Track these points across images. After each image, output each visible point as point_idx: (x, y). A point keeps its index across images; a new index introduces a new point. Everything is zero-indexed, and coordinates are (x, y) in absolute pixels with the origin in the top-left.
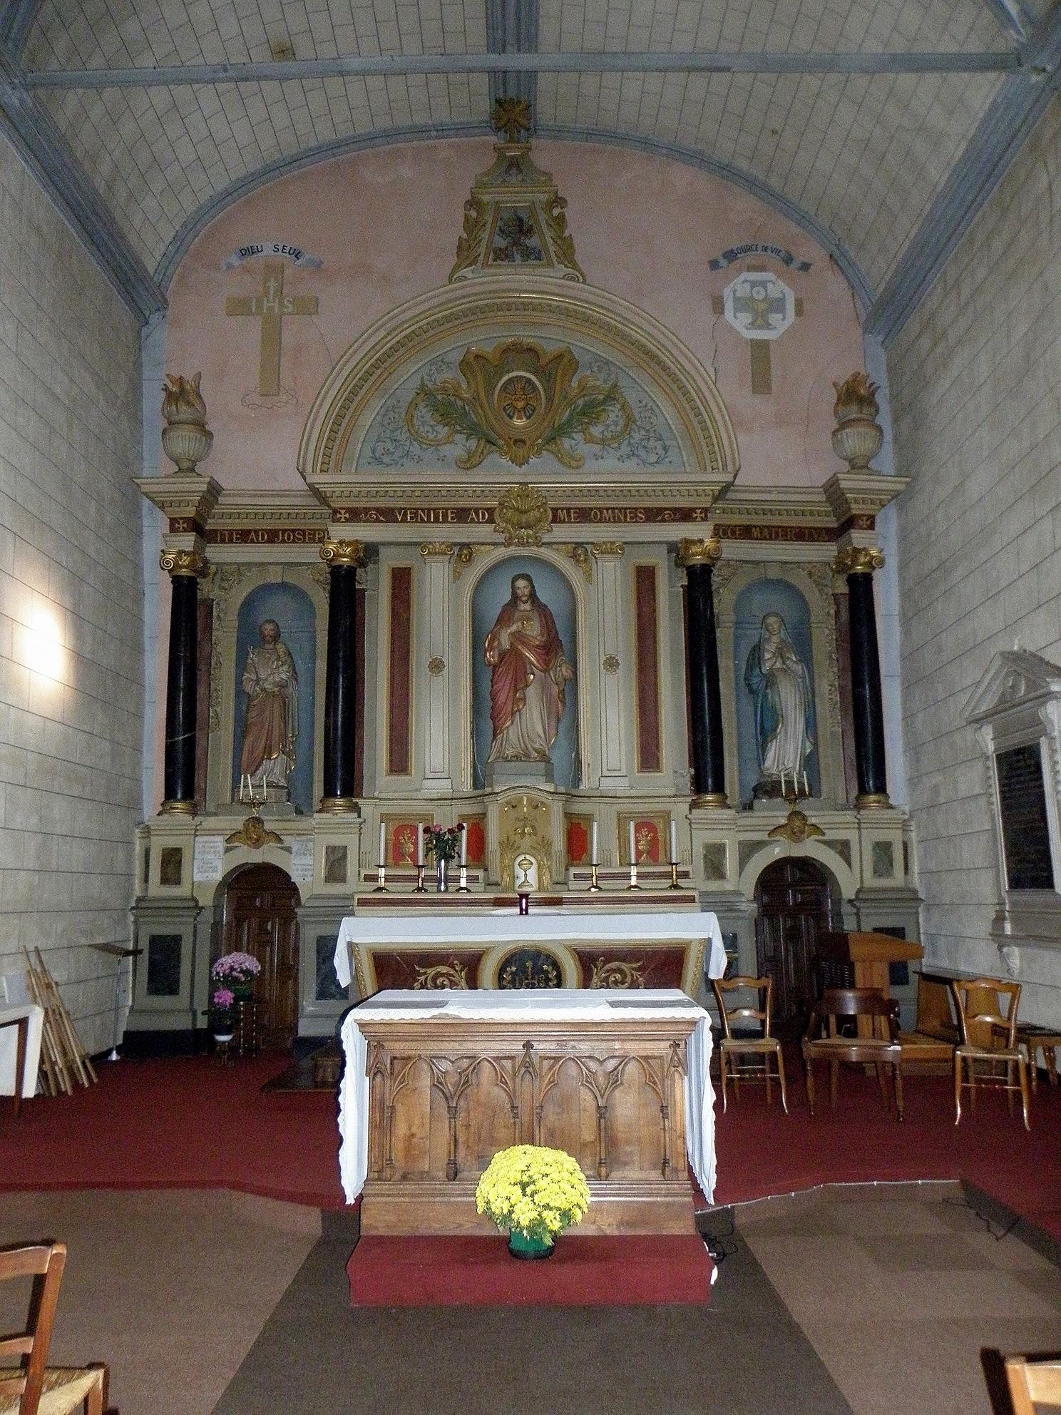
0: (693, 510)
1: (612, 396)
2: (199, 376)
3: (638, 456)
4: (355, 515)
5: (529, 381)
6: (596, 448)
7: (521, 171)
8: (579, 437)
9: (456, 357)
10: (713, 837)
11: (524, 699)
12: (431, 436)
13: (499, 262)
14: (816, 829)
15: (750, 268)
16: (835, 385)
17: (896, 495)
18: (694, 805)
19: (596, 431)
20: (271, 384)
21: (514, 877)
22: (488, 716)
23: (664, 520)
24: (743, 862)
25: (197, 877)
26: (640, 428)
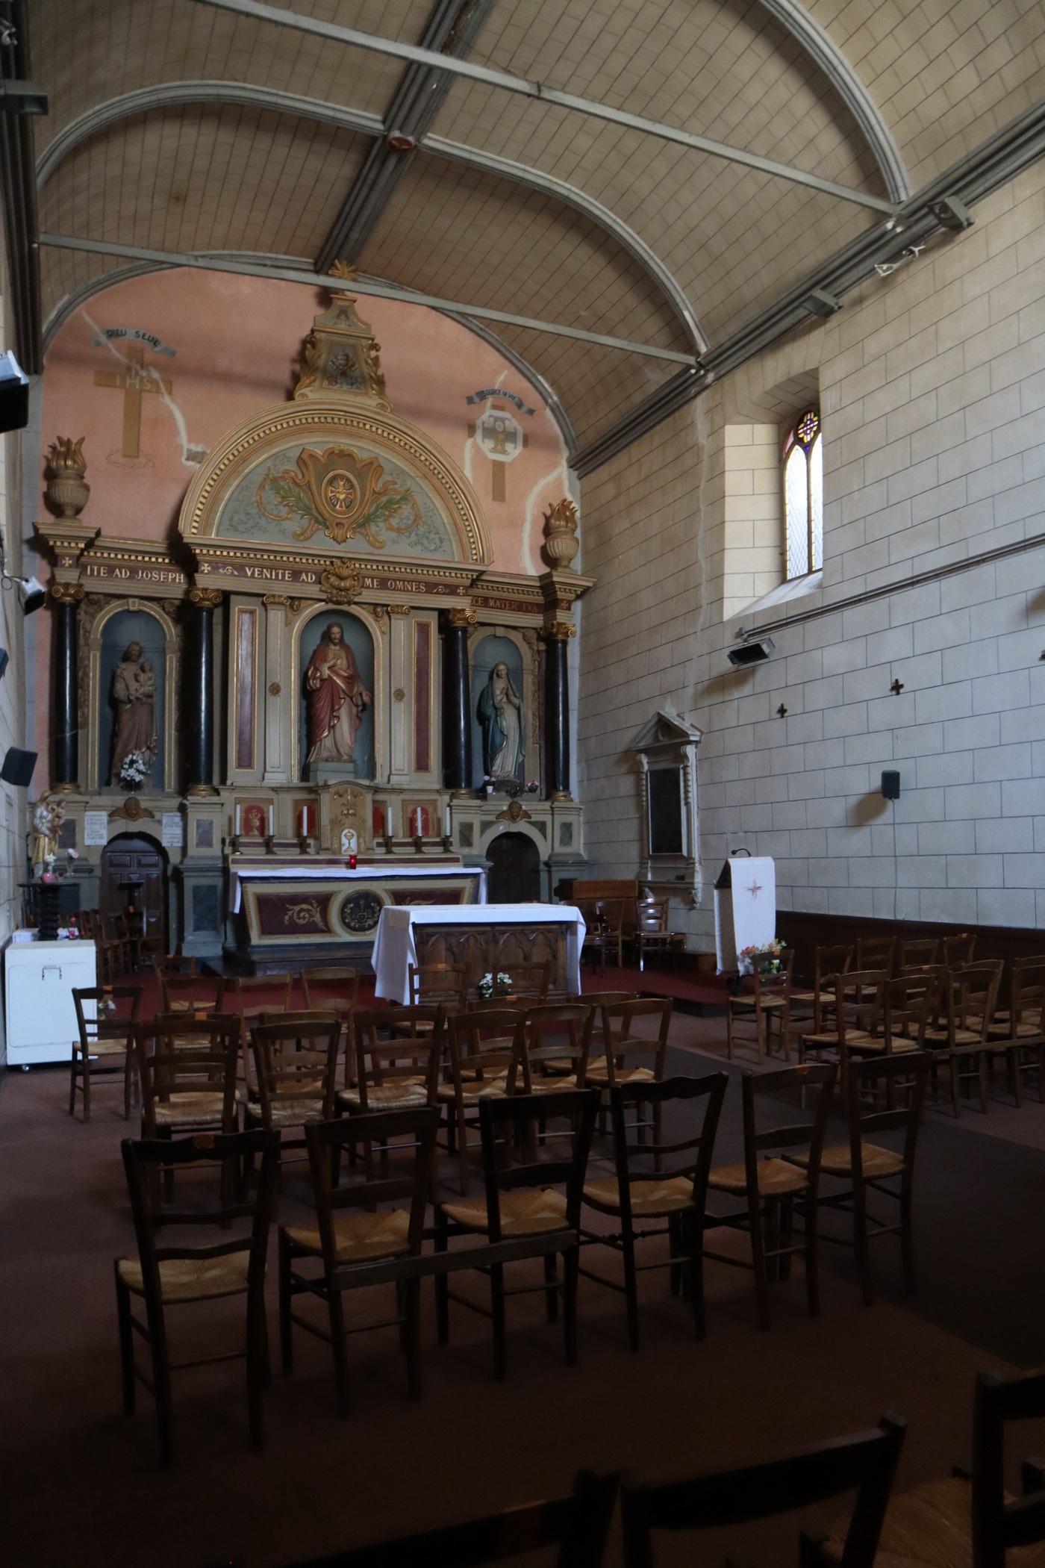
0: (458, 587)
1: (405, 497)
2: (82, 440)
4: (215, 567)
5: (348, 480)
6: (394, 535)
8: (381, 525)
9: (295, 454)
10: (466, 818)
11: (338, 718)
14: (527, 815)
15: (494, 407)
17: (586, 590)
18: (453, 797)
19: (394, 522)
21: (340, 845)
22: (311, 730)
23: (438, 593)
24: (482, 832)
25: (87, 842)
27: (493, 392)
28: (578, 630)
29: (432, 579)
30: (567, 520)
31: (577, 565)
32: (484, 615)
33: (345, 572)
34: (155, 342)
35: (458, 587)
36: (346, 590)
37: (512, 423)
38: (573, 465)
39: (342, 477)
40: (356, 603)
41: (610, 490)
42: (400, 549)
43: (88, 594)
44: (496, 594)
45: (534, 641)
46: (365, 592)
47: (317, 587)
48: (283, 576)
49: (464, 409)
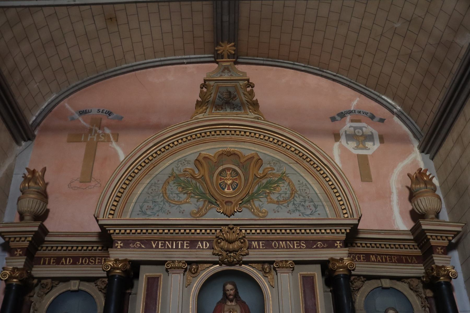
0: (335, 241)
2: (44, 170)
3: (299, 210)
4: (127, 244)
5: (234, 170)
6: (275, 206)
7: (230, 71)
8: (264, 200)
9: (194, 157)
12: (176, 199)
13: (218, 111)
15: (352, 121)
16: (409, 175)
19: (274, 197)
20: (87, 177)
23: (317, 247)
26: (299, 195)
27: (350, 112)
28: (459, 269)
29: (310, 237)
30: (425, 183)
31: (444, 215)
32: (362, 268)
33: (232, 236)
34: (110, 113)
35: (335, 241)
36: (234, 251)
37: (368, 128)
38: (423, 150)
39: (228, 169)
40: (246, 263)
41: (457, 151)
42: (281, 215)
43: (40, 279)
44: (375, 250)
45: (421, 290)
46: (251, 252)
47: (210, 252)
48: (182, 245)
49: (329, 125)
